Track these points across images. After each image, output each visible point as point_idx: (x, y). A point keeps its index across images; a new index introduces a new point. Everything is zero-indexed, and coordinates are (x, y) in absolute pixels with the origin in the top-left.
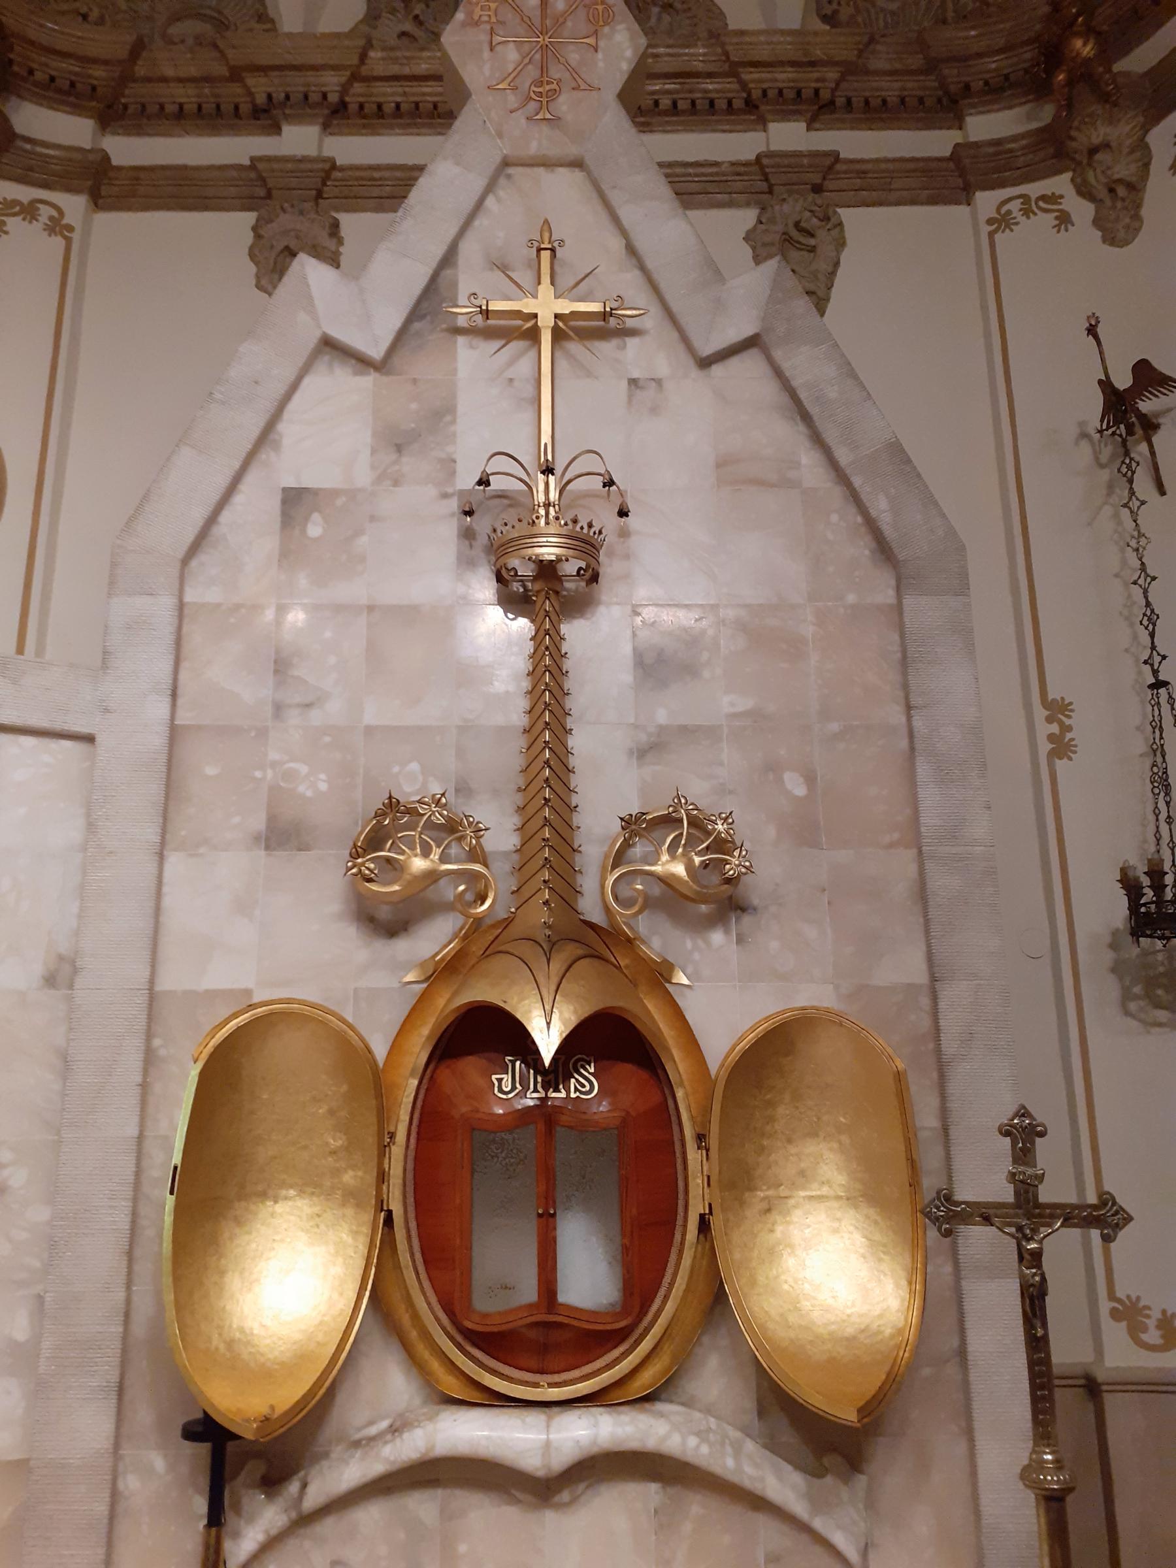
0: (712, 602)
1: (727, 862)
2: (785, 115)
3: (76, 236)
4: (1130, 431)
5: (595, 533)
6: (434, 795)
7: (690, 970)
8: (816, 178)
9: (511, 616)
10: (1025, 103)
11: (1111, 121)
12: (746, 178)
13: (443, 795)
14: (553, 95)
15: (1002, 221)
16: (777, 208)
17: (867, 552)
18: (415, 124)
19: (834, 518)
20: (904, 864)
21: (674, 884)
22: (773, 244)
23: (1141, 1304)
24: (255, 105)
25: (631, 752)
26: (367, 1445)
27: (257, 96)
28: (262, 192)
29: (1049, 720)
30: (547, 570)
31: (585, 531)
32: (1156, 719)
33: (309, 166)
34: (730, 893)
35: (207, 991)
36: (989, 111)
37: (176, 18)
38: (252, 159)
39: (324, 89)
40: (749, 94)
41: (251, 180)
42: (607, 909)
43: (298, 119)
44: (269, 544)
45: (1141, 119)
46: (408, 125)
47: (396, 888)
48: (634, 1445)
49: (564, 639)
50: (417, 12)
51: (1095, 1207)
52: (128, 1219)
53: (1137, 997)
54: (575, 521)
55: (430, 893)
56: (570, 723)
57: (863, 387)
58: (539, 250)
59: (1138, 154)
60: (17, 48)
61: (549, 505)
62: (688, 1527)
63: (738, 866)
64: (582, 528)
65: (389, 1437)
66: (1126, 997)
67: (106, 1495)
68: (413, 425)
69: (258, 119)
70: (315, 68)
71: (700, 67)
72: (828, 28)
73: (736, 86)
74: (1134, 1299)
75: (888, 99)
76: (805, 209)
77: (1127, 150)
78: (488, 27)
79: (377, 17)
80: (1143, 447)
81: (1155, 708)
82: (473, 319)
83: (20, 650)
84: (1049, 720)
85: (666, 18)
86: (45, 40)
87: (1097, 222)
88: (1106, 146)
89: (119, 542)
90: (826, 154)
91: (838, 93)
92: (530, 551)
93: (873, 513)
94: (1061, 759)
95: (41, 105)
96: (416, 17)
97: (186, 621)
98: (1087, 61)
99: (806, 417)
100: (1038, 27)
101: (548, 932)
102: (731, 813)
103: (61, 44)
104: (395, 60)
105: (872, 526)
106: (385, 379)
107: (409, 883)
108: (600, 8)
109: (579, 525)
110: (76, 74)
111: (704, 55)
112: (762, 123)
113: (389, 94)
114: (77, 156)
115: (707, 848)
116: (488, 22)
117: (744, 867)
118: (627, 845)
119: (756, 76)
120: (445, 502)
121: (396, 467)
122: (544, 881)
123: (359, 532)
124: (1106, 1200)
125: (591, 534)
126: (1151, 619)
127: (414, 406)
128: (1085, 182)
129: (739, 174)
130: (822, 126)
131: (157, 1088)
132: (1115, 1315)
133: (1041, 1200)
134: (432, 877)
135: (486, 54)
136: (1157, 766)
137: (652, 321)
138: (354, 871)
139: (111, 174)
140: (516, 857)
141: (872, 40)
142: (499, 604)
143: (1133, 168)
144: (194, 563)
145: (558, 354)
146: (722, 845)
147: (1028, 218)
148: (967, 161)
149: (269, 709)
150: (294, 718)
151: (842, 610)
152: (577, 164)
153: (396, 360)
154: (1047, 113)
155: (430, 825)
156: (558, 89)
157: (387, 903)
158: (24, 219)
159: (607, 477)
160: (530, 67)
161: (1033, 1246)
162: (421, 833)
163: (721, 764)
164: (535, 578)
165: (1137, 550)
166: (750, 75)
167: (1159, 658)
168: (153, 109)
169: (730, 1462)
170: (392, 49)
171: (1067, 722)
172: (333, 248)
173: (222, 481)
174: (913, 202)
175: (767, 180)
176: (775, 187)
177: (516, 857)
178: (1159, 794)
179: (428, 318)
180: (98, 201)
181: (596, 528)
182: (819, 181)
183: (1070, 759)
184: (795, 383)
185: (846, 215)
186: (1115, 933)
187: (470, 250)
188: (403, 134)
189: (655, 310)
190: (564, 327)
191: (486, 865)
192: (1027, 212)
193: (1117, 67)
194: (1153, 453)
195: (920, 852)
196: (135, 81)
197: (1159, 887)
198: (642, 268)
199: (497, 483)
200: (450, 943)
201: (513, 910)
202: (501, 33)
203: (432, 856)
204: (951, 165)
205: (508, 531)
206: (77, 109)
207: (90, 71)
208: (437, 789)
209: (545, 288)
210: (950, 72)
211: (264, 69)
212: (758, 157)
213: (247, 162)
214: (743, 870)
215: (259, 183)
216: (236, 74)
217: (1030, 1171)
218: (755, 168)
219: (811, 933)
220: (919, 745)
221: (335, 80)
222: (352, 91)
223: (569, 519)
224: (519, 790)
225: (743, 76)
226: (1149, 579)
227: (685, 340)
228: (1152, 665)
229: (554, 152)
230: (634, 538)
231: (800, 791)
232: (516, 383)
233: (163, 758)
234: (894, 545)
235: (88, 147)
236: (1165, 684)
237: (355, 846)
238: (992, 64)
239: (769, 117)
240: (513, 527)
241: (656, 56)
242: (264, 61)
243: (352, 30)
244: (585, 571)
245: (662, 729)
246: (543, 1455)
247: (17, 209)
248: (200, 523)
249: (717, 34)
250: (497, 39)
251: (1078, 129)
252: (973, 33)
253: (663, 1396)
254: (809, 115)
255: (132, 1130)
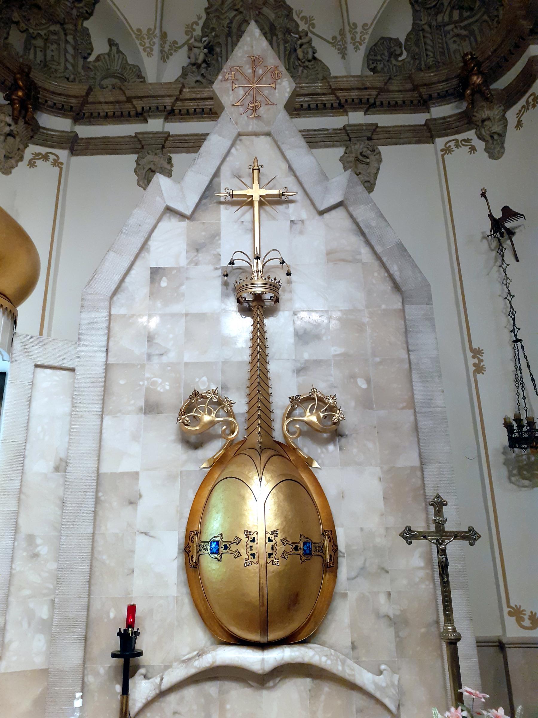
0: (326, 309)
1: (334, 416)
2: (355, 109)
3: (64, 167)
4: (502, 235)
5: (277, 282)
6: (213, 390)
7: (320, 461)
8: (369, 135)
9: (244, 317)
10: (455, 102)
11: (490, 108)
12: (339, 135)
13: (216, 389)
14: (258, 107)
15: (447, 150)
16: (353, 147)
17: (390, 288)
18: (202, 117)
19: (376, 274)
20: (408, 416)
21: (312, 425)
22: (351, 162)
23: (521, 609)
24: (137, 112)
25: (294, 371)
26: (188, 661)
27: (138, 108)
28: (140, 146)
29: (473, 357)
30: (258, 298)
31: (273, 281)
32: (516, 355)
33: (159, 135)
34: (335, 429)
35: (121, 473)
36: (442, 105)
37: (105, 77)
38: (136, 133)
39: (165, 105)
40: (340, 101)
41: (135, 142)
42: (285, 437)
43: (155, 117)
44: (146, 290)
45: (502, 108)
46: (200, 118)
47: (198, 428)
48: (299, 660)
49: (265, 325)
50: (202, 72)
51: (466, 532)
52: (89, 567)
53: (515, 475)
54: (269, 278)
55: (211, 430)
56: (268, 359)
57: (387, 221)
58: (253, 170)
59: (502, 122)
60: (41, 92)
61: (258, 271)
62: (323, 697)
63: (338, 417)
64: (272, 280)
65: (197, 658)
66: (510, 475)
67: (80, 683)
68: (203, 241)
69: (138, 117)
70: (162, 96)
71: (319, 91)
72: (373, 73)
73: (334, 98)
74: (518, 607)
75: (398, 102)
76: (365, 147)
77: (497, 120)
78: (232, 81)
79: (186, 75)
80: (509, 242)
81: (516, 350)
82: (227, 198)
83: (41, 333)
84: (473, 357)
85: (305, 71)
86: (52, 89)
87: (487, 150)
88: (489, 119)
89: (85, 290)
90: (372, 125)
91: (377, 100)
92: (251, 290)
93: (391, 272)
94: (478, 373)
95: (50, 114)
96: (202, 75)
97: (112, 321)
98: (479, 85)
99: (363, 234)
100: (459, 71)
101: (260, 445)
102: (335, 395)
103: (59, 90)
104: (194, 92)
105: (391, 277)
106: (192, 223)
107: (203, 426)
108: (276, 72)
109: (271, 279)
110: (65, 102)
111: (321, 86)
112: (346, 113)
113: (192, 105)
114: (64, 134)
115: (326, 410)
116: (232, 79)
117: (341, 417)
118: (293, 409)
119: (343, 94)
120: (217, 271)
121: (197, 258)
122: (258, 424)
123: (182, 284)
124: (471, 529)
125: (276, 283)
126: (513, 313)
127: (203, 233)
128: (481, 134)
129: (336, 134)
130: (371, 113)
131: (100, 513)
132: (510, 614)
133: (445, 530)
134: (212, 423)
135: (231, 92)
136: (517, 375)
137: (299, 197)
138: (181, 421)
139: (79, 141)
140: (246, 415)
141: (390, 78)
142: (238, 312)
143: (501, 127)
144: (115, 298)
145: (261, 211)
146: (332, 409)
147: (458, 148)
148: (431, 126)
149: (145, 356)
150: (155, 360)
151: (380, 312)
152: (268, 134)
153: (196, 215)
154: (464, 106)
155: (211, 403)
156: (260, 105)
157: (194, 434)
158: (43, 161)
159: (281, 260)
160: (248, 96)
161: (443, 547)
162: (208, 405)
163: (332, 376)
164: (253, 301)
165: (506, 285)
166: (340, 94)
167: (517, 330)
168: (95, 114)
169: (340, 668)
170: (193, 88)
171: (481, 358)
172: (169, 168)
173: (126, 265)
174: (410, 143)
175: (348, 135)
176: (352, 138)
177: (246, 415)
178: (518, 387)
179: (209, 198)
180: (73, 152)
181: (277, 280)
182: (370, 136)
183: (483, 373)
184: (358, 220)
185: (381, 149)
186: (504, 448)
187: (225, 171)
188: (197, 121)
189: (300, 192)
190: (264, 200)
191: (234, 418)
192: (457, 146)
193: (492, 87)
194: (513, 245)
195: (415, 411)
196: (88, 103)
197: (520, 426)
198: (296, 176)
199: (237, 263)
200: (220, 451)
201: (246, 437)
202: (237, 83)
203: (212, 415)
204: (425, 127)
205: (242, 282)
206: (65, 116)
207: (70, 101)
208: (214, 387)
209: (256, 185)
210: (423, 90)
211: (141, 98)
212: (344, 126)
213: (134, 135)
214: (341, 419)
215: (139, 143)
216: (129, 100)
217: (441, 519)
218: (343, 131)
219: (370, 445)
220: (413, 367)
221: (170, 101)
222: (176, 105)
223: (266, 276)
224: (248, 387)
225: (337, 94)
226: (511, 297)
227: (313, 204)
228: (514, 333)
229: (258, 129)
230: (293, 285)
231: (364, 386)
232: (244, 223)
233: (103, 377)
234: (400, 285)
235: (69, 130)
236: (520, 340)
237: (181, 411)
238: (441, 86)
239: (348, 110)
240: (244, 281)
241: (302, 87)
242: (140, 94)
243: (176, 80)
244: (273, 297)
245: (306, 361)
246: (261, 664)
247: (41, 156)
248: (117, 282)
249: (326, 78)
250: (235, 86)
251: (477, 112)
252: (432, 74)
253: (312, 641)
254: (365, 109)
255: (90, 531)
